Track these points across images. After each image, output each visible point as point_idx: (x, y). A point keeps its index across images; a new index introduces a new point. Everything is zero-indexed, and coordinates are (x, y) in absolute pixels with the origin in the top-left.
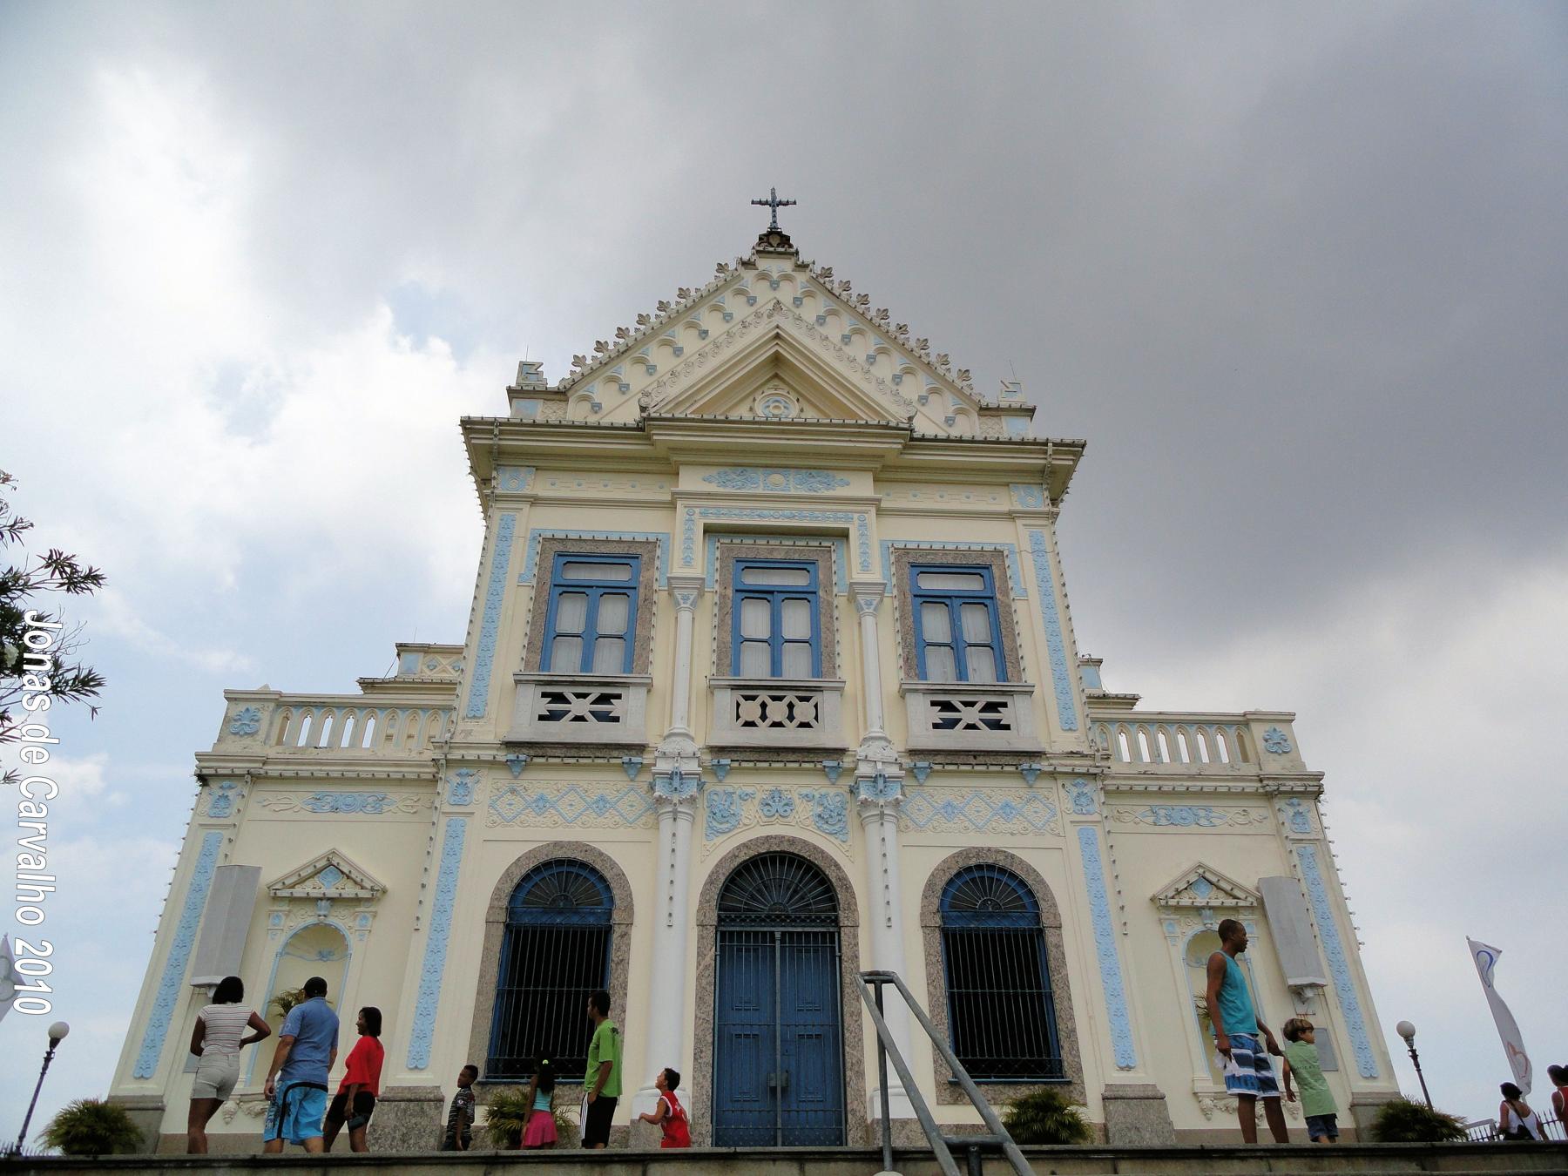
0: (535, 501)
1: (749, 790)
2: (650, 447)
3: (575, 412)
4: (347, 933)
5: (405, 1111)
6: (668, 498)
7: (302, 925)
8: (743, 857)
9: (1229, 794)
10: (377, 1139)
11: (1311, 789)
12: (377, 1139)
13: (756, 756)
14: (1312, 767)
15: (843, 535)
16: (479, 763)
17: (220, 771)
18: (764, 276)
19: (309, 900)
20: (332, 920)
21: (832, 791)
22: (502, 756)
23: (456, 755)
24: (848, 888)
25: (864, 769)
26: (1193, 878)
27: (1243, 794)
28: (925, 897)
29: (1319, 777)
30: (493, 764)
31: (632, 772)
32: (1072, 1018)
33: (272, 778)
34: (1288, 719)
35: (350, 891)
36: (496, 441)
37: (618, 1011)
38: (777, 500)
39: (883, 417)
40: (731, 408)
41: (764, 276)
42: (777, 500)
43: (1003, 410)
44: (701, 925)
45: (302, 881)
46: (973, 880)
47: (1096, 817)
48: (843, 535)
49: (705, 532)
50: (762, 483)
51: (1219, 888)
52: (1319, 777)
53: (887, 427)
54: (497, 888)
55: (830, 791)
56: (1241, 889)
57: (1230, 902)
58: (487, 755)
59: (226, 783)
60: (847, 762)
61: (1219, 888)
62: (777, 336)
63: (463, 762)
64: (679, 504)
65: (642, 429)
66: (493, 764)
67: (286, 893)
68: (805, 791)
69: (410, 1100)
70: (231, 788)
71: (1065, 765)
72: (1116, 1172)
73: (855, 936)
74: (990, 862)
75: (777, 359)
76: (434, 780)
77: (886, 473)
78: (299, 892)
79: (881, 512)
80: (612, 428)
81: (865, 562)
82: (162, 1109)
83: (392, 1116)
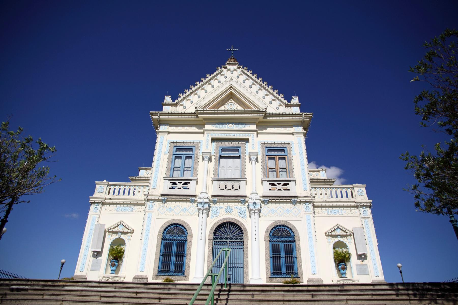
0: (169, 133)
6: (202, 131)
9: (347, 207)
16: (155, 200)
19: (116, 233)
24: (246, 231)
25: (251, 201)
27: (351, 207)
28: (266, 233)
30: (158, 200)
32: (301, 262)
35: (126, 230)
48: (247, 140)
51: (342, 230)
62: (231, 87)
73: (247, 242)
74: (283, 224)
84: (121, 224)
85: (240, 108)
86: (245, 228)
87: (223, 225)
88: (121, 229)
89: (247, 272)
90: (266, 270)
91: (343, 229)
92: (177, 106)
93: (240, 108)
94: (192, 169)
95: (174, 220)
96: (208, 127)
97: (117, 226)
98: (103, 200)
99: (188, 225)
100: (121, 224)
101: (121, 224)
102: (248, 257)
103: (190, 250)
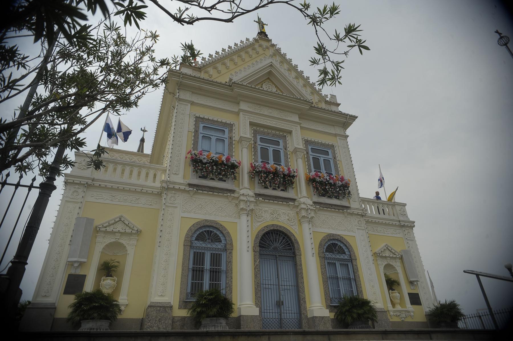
0: (193, 103)
1: (267, 209)
2: (231, 93)
3: (203, 75)
4: (127, 246)
5: (159, 310)
6: (237, 111)
7: (109, 242)
8: (266, 230)
10: (150, 321)
11: (411, 225)
12: (150, 321)
13: (269, 198)
14: (411, 219)
15: (290, 132)
16: (179, 190)
17: (75, 182)
18: (260, 46)
19: (113, 233)
20: (121, 241)
21: (291, 212)
22: (187, 188)
23: (171, 186)
24: (297, 243)
25: (303, 206)
26: (385, 248)
28: (319, 247)
29: (414, 222)
30: (184, 191)
31: (230, 199)
32: (361, 287)
33: (127, 190)
34: (404, 205)
35: (128, 230)
36: (181, 80)
37: (230, 278)
38: (272, 118)
39: (303, 97)
40: (257, 85)
41: (260, 46)
42: (272, 118)
43: (332, 103)
44: (254, 251)
45: (110, 225)
46: (288, 242)
47: (363, 228)
48: (290, 132)
49: (250, 124)
50: (266, 111)
51: (391, 252)
52: (414, 222)
53: (306, 101)
54: (187, 234)
55: (292, 213)
56: (397, 252)
57: (395, 256)
58: (182, 187)
59: (77, 186)
60: (296, 203)
61: (391, 252)
62: (271, 65)
63: (174, 189)
64: (241, 113)
65: (231, 86)
66: (184, 191)
67: (104, 229)
68: (283, 211)
69: (161, 307)
70: (79, 188)
71: (356, 212)
72: (431, 339)
73: (301, 258)
75: (270, 73)
76: (159, 194)
77: (303, 116)
78: (109, 229)
79: (301, 128)
80: (216, 82)
81: (213, 139)
82: (55, 308)
83: (155, 312)
84: (120, 220)
85: (274, 90)
86: (296, 240)
87: (272, 233)
88: (119, 227)
89: (305, 298)
90: (325, 295)
91: (392, 251)
92: (201, 72)
93: (274, 90)
94: (140, 153)
95: (206, 220)
96: (243, 106)
97: (113, 224)
98: (90, 182)
99: (226, 229)
100: (120, 220)
101: (120, 220)
102: (303, 278)
103: (231, 265)
